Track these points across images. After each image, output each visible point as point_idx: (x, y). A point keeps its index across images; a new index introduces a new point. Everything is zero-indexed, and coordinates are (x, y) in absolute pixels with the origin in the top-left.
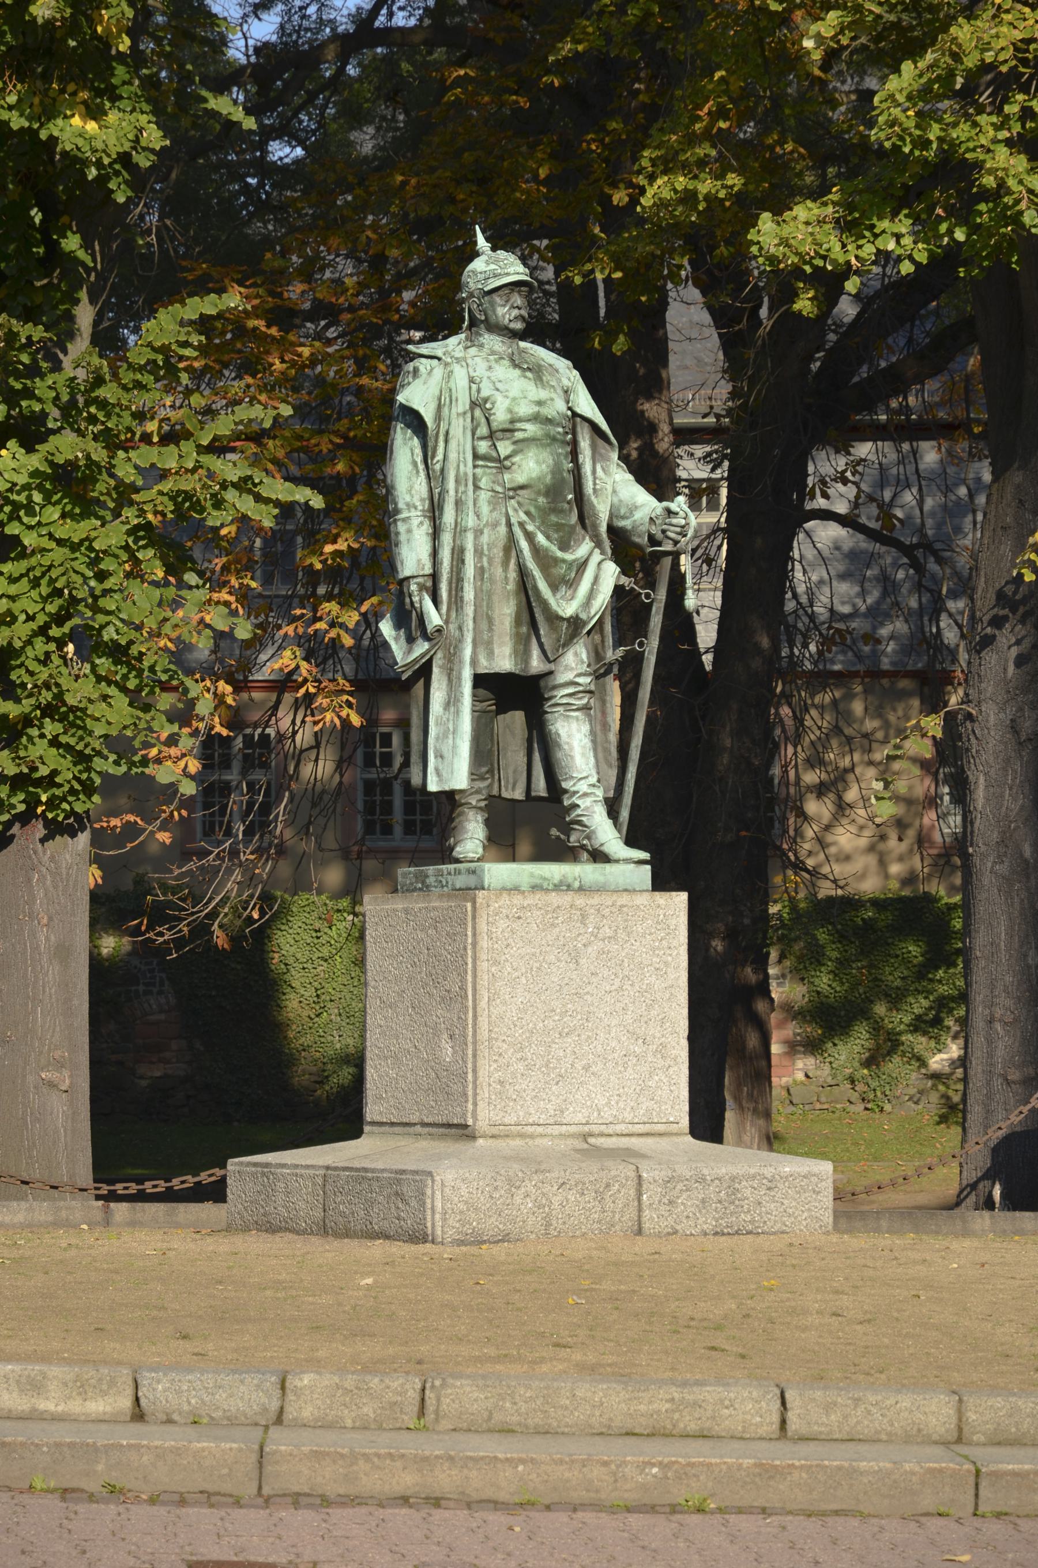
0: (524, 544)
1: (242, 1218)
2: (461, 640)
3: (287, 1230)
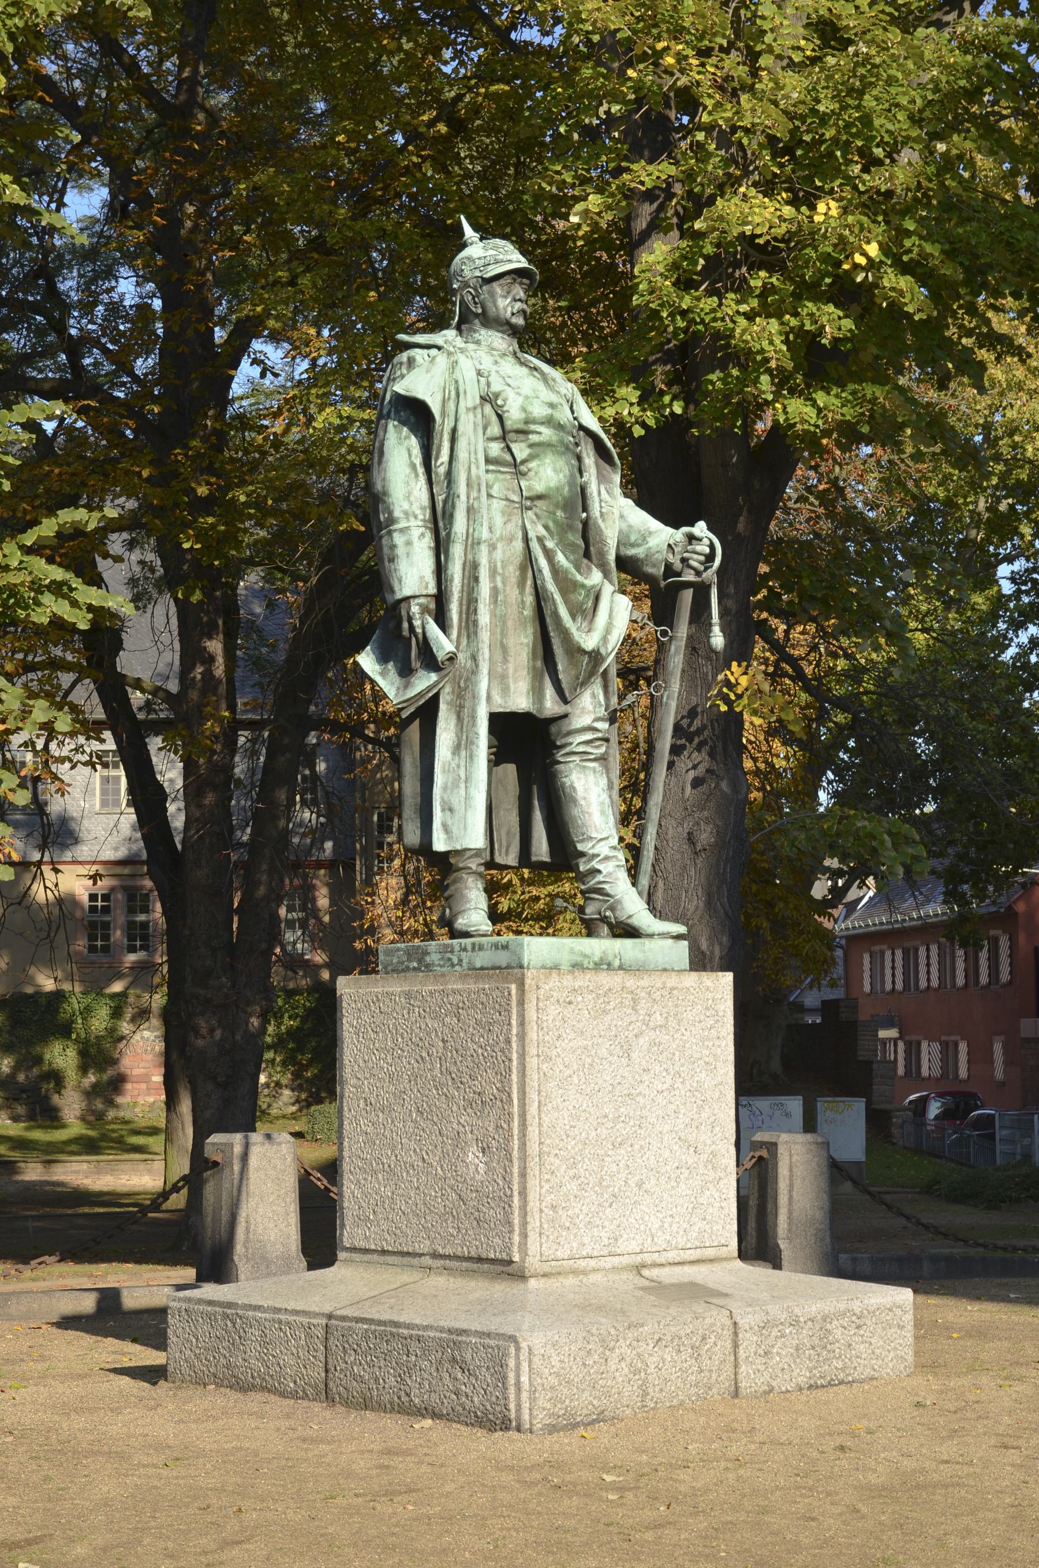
0: (543, 563)
1: (191, 1367)
2: (475, 671)
3: (263, 1389)
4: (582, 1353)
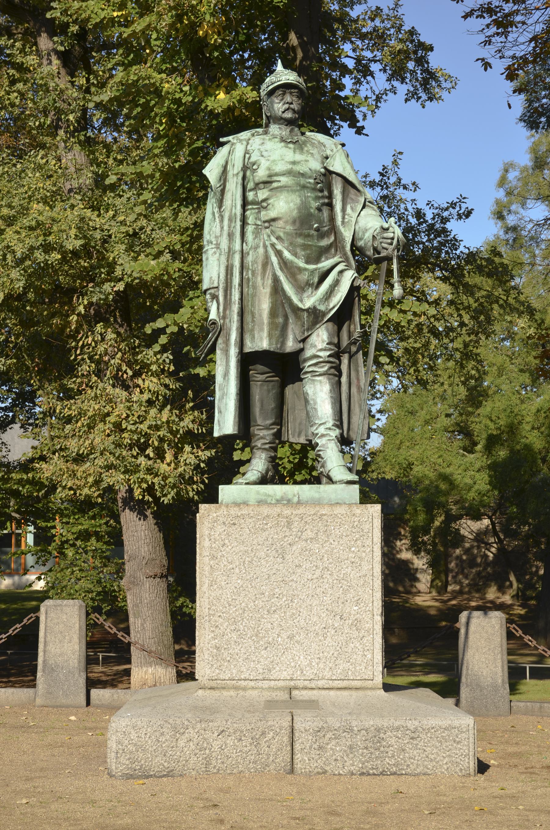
4: (158, 734)
